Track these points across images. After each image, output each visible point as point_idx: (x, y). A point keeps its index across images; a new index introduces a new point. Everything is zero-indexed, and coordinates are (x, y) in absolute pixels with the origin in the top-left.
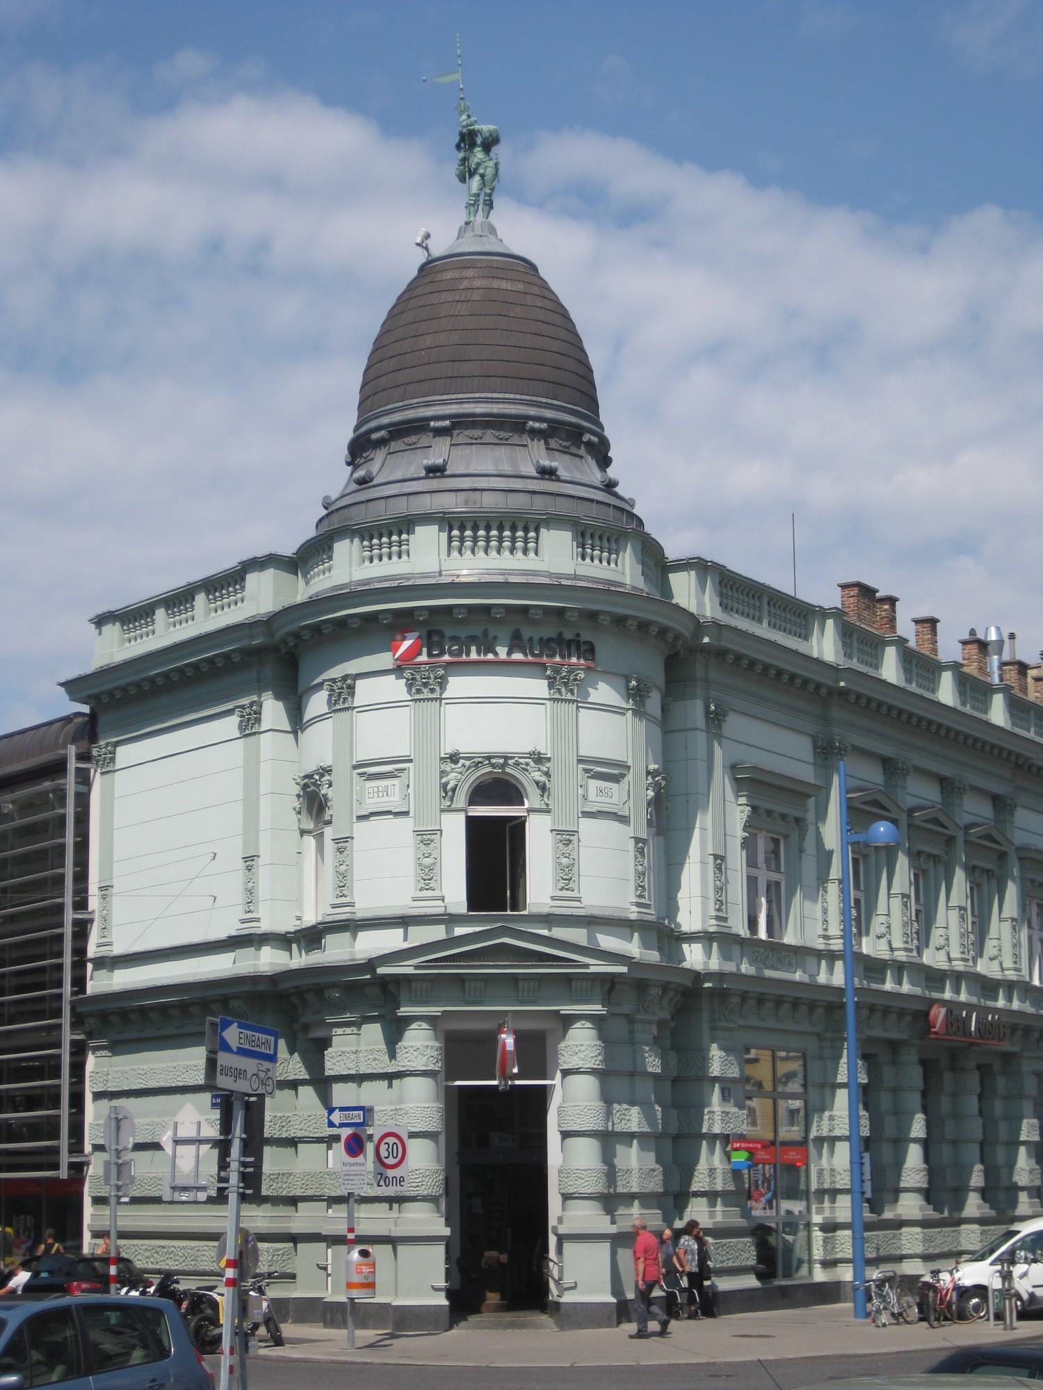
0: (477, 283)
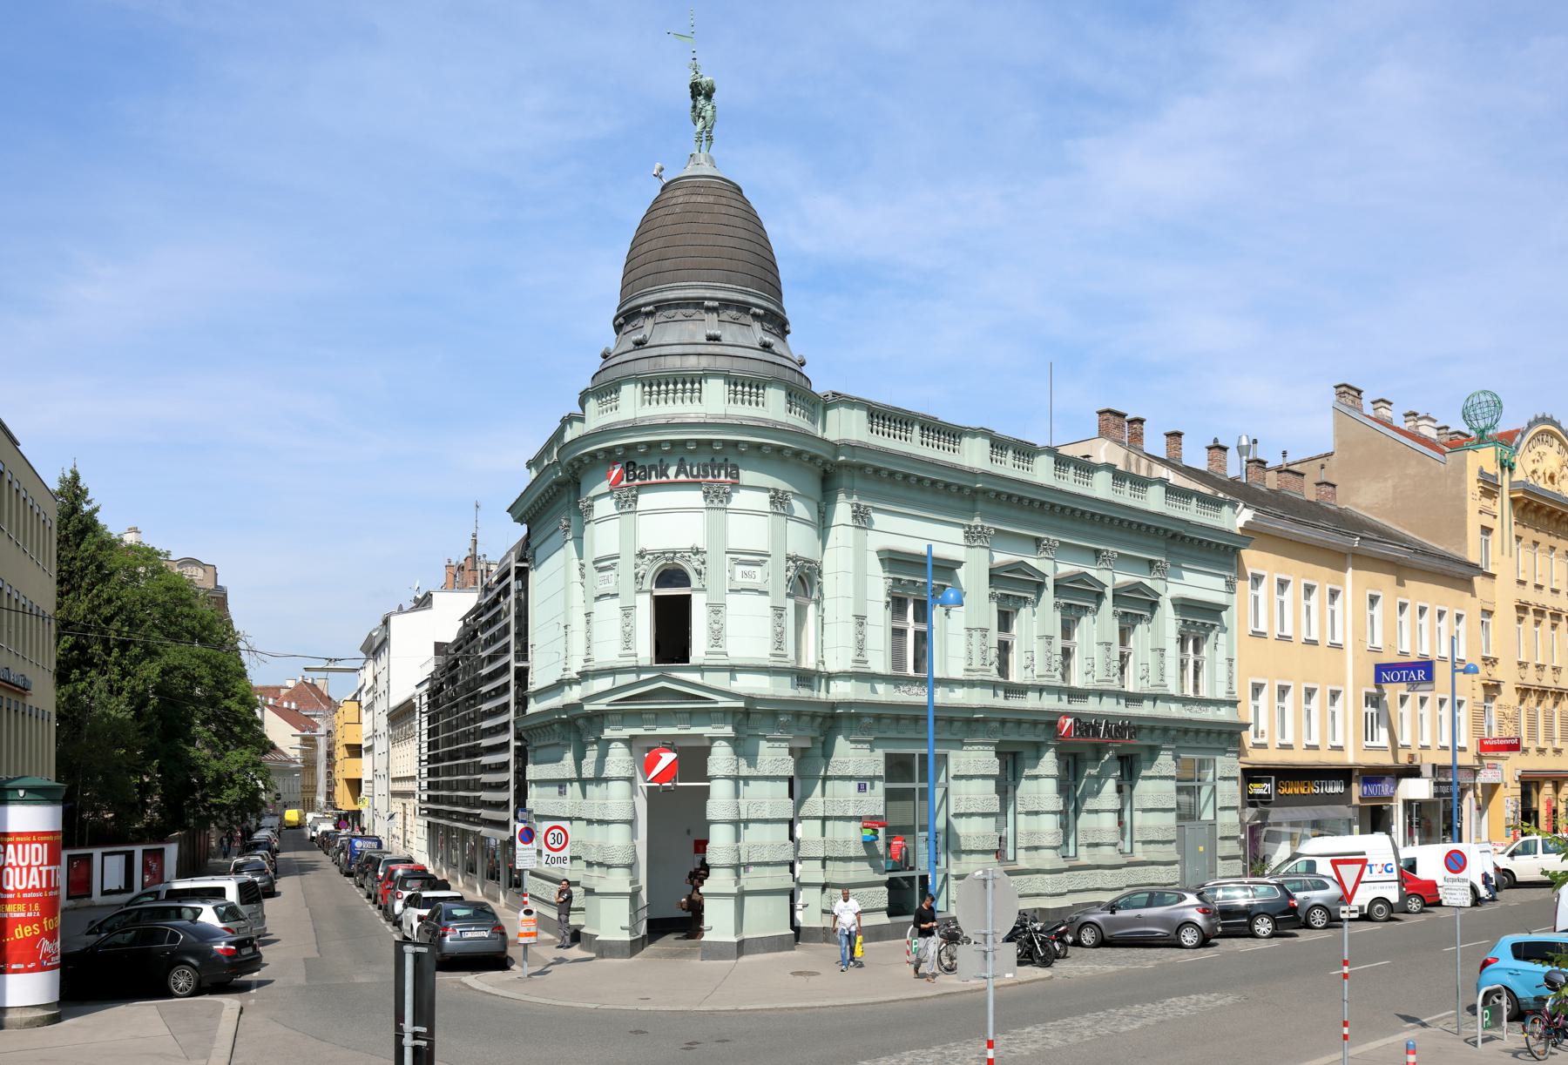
0: (681, 200)
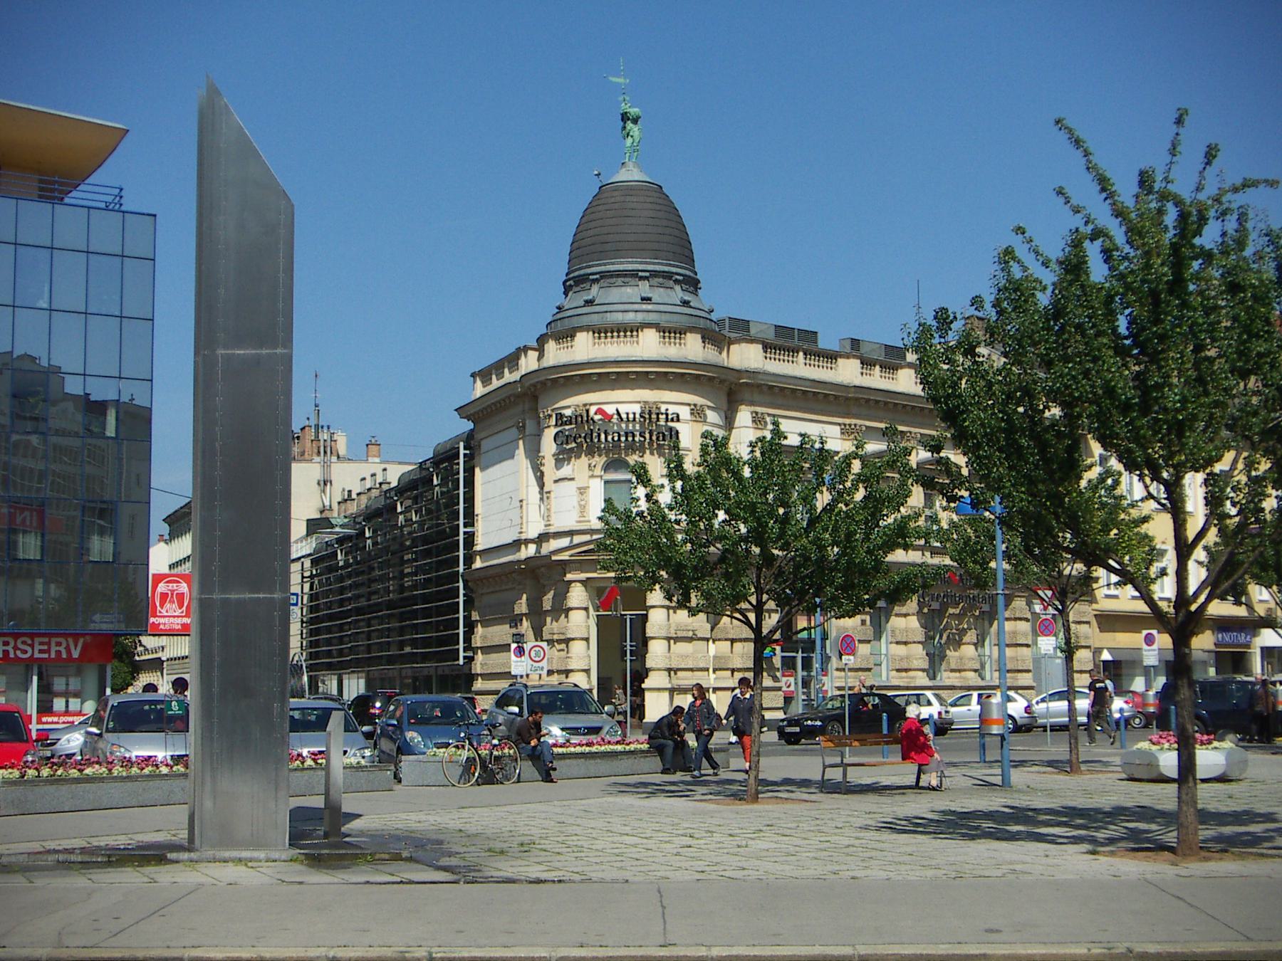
0: (618, 199)
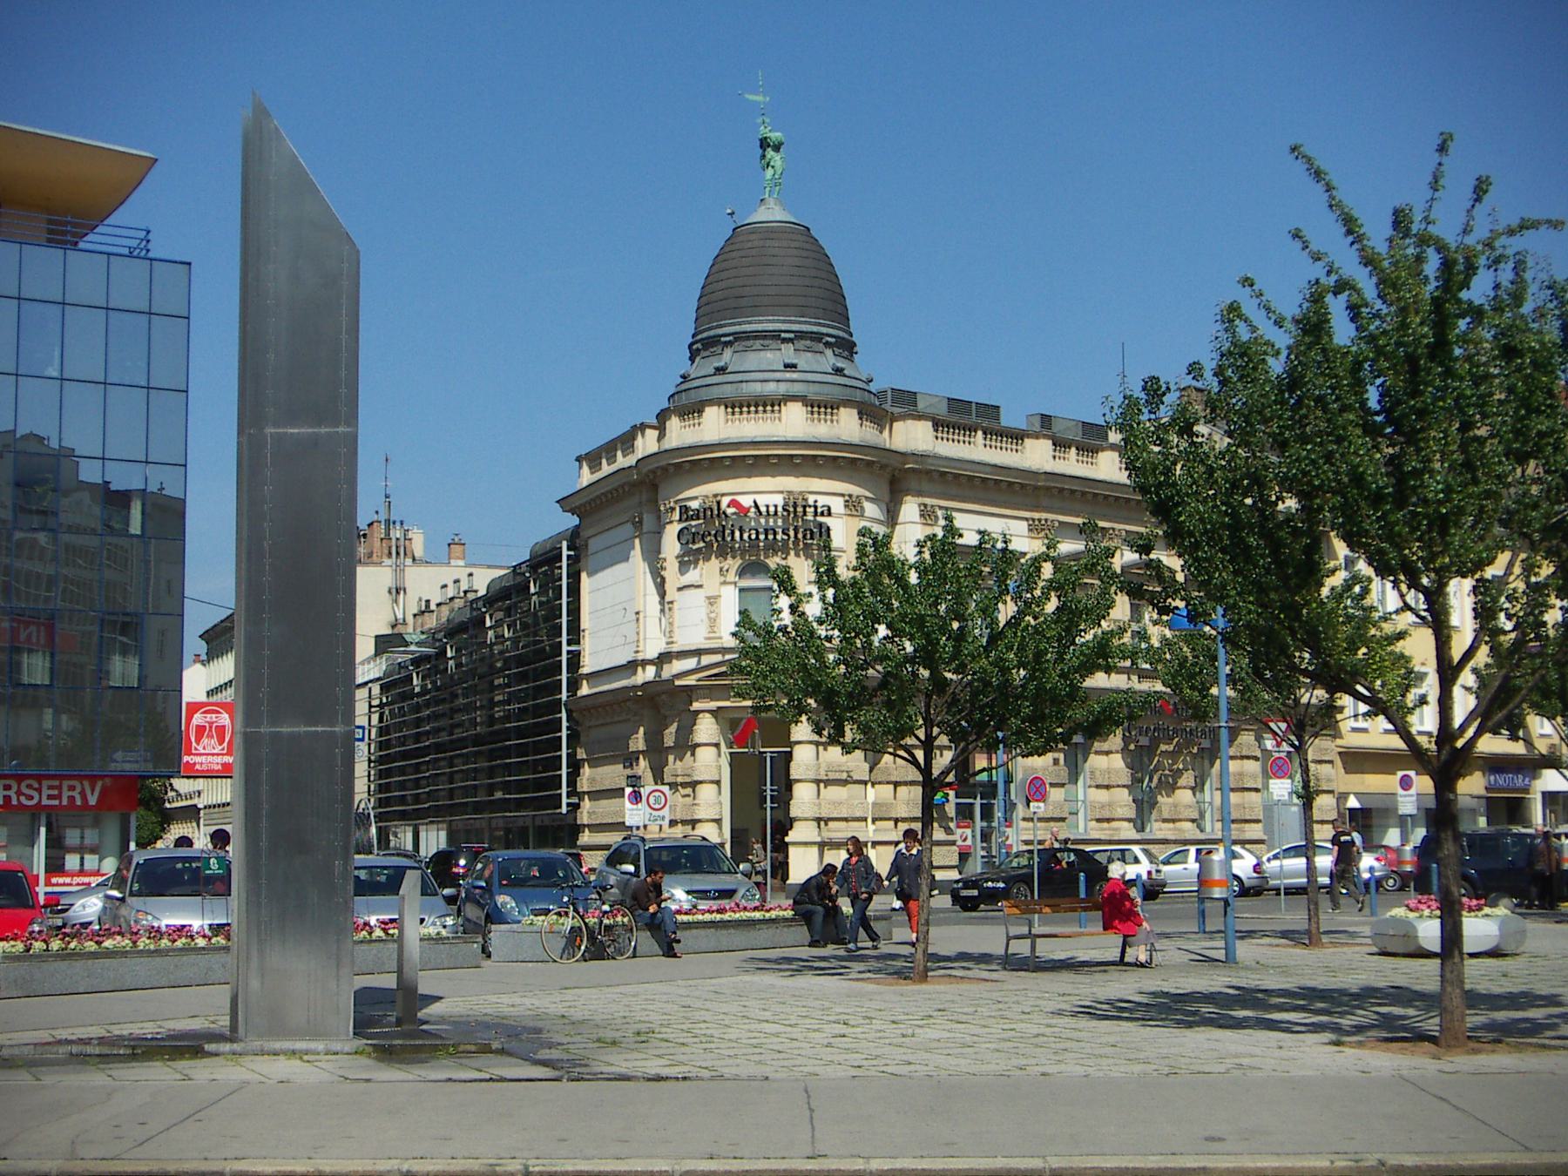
0: (756, 243)
